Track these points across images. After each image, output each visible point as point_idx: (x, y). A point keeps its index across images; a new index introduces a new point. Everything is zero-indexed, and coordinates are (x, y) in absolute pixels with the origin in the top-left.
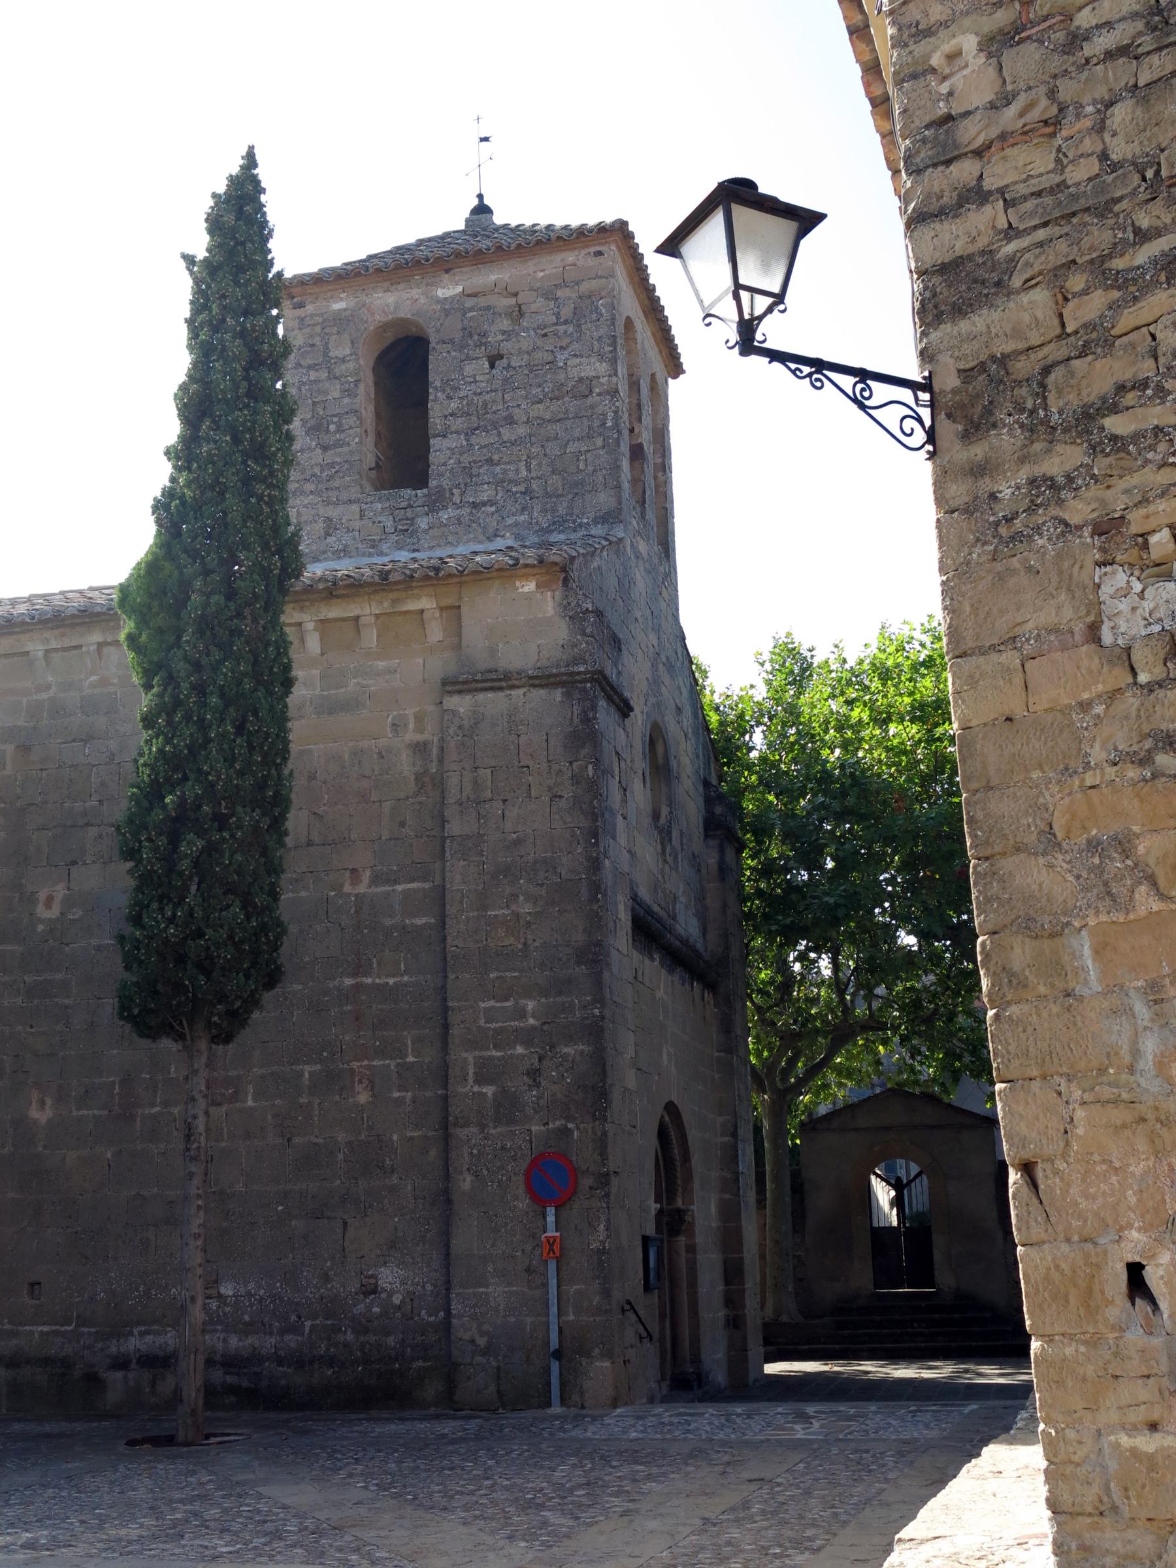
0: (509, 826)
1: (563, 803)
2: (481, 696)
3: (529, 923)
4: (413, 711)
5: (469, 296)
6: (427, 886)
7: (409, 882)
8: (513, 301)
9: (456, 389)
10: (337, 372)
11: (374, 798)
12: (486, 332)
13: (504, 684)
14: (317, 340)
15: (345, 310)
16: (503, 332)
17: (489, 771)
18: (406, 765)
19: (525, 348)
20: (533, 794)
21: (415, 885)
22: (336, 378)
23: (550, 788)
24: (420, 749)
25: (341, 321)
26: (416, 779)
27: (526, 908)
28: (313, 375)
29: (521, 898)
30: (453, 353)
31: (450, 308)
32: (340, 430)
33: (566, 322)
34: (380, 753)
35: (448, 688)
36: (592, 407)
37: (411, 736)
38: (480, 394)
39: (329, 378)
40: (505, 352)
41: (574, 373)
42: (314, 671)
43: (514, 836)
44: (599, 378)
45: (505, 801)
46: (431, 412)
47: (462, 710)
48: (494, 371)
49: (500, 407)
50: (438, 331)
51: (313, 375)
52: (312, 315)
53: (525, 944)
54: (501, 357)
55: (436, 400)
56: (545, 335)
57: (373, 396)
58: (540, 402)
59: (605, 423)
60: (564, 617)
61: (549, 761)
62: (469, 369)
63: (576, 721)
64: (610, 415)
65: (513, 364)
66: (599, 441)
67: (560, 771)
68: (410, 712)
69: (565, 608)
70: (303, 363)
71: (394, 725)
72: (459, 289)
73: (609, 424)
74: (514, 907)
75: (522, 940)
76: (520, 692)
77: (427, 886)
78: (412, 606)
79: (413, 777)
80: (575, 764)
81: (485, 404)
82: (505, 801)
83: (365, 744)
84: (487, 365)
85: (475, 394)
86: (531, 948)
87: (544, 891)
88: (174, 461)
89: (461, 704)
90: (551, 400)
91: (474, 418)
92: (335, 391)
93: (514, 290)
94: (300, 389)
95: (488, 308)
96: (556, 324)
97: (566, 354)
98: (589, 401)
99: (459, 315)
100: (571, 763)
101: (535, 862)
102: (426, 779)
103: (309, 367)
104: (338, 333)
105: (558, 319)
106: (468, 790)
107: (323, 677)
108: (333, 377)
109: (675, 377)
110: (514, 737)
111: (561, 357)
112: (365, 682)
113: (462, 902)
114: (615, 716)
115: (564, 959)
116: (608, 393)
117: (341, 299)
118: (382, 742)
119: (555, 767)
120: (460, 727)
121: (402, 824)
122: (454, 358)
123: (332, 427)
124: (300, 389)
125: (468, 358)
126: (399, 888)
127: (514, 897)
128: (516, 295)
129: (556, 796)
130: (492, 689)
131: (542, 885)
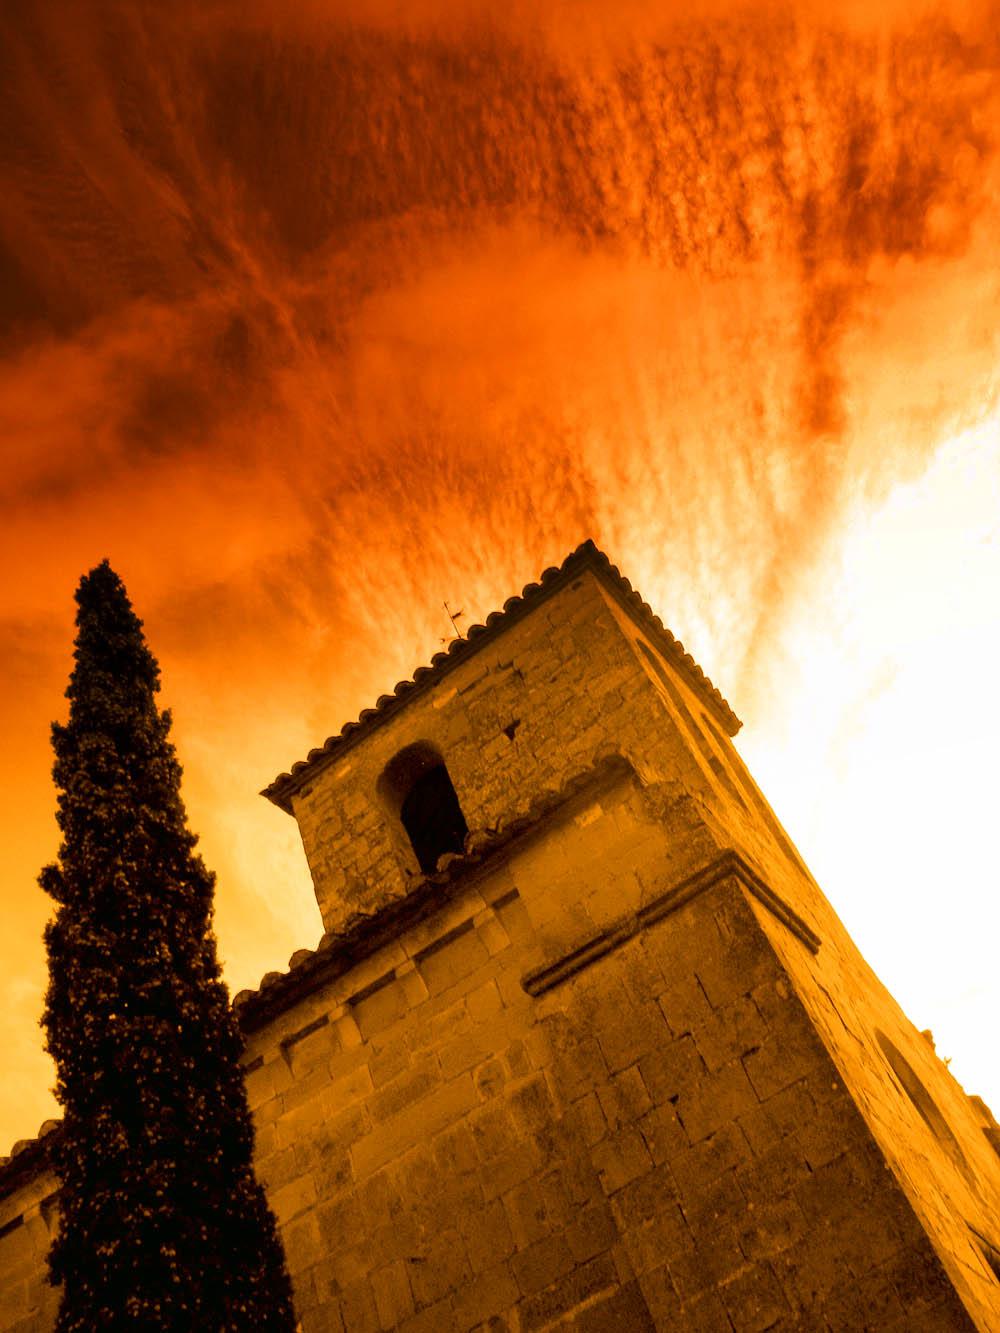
0: (695, 1133)
1: (762, 1057)
2: (584, 978)
3: (792, 1269)
4: (502, 1052)
5: (464, 692)
6: (610, 1292)
7: (582, 1298)
8: (511, 670)
9: (481, 778)
10: (359, 829)
11: (489, 1197)
12: (493, 712)
13: (607, 943)
14: (332, 813)
15: (351, 771)
16: (512, 701)
17: (635, 1068)
18: (518, 1128)
19: (538, 701)
20: (711, 1065)
21: (592, 1300)
22: (360, 835)
23: (734, 1046)
24: (531, 1097)
25: (350, 785)
26: (539, 1139)
27: (776, 1247)
28: (337, 845)
29: (762, 1233)
30: (468, 748)
31: (448, 714)
32: (379, 878)
33: (569, 658)
34: (477, 1130)
35: (535, 988)
36: (631, 711)
37: (513, 1085)
38: (509, 766)
39: (353, 839)
40: (520, 716)
41: (599, 693)
42: (361, 1068)
43: (710, 1144)
44: (625, 683)
45: (674, 1100)
46: (465, 812)
47: (563, 1009)
48: (516, 739)
49: (534, 766)
50: (446, 738)
51: (337, 845)
52: (320, 795)
53: (802, 1309)
54: (517, 723)
55: (466, 797)
56: (554, 680)
57: (408, 841)
58: (574, 737)
59: (652, 718)
60: (654, 823)
61: (715, 1009)
62: (489, 752)
63: (729, 935)
64: (654, 707)
65: (531, 721)
66: (654, 736)
67: (737, 1014)
68: (499, 1056)
69: (651, 811)
70: (323, 840)
71: (484, 1083)
72: (454, 691)
73: (657, 715)
74: (756, 1254)
75: (794, 1304)
76: (635, 942)
77: (610, 1292)
78: (455, 922)
79: (533, 1140)
80: (754, 995)
81: (519, 773)
82: (674, 1100)
83: (454, 1129)
84: (506, 738)
85: (503, 769)
86: (816, 1311)
87: (794, 1206)
88: (68, 831)
89: (561, 1001)
90: (585, 729)
91: (512, 791)
92: (362, 846)
93: (506, 661)
94: (327, 865)
95: (489, 689)
96: (562, 664)
97: (583, 682)
98: (625, 709)
99: (462, 712)
100: (748, 995)
101: (760, 1167)
102: (553, 1134)
103: (332, 839)
104: (350, 795)
105: (560, 659)
106: (614, 1111)
107: (374, 1070)
108: (356, 836)
109: (733, 733)
110: (651, 1004)
111: (579, 691)
112: (428, 1049)
113: (671, 1288)
114: (804, 952)
115: (880, 1303)
116: (641, 691)
117: (344, 765)
118: (475, 1115)
119: (728, 1014)
120: (571, 1032)
121: (541, 1215)
122: (472, 750)
123: (370, 882)
124: (327, 865)
125: (485, 743)
126: (570, 1316)
127: (749, 1236)
128: (511, 664)
129: (747, 1053)
130: (596, 958)
131: (786, 1197)
